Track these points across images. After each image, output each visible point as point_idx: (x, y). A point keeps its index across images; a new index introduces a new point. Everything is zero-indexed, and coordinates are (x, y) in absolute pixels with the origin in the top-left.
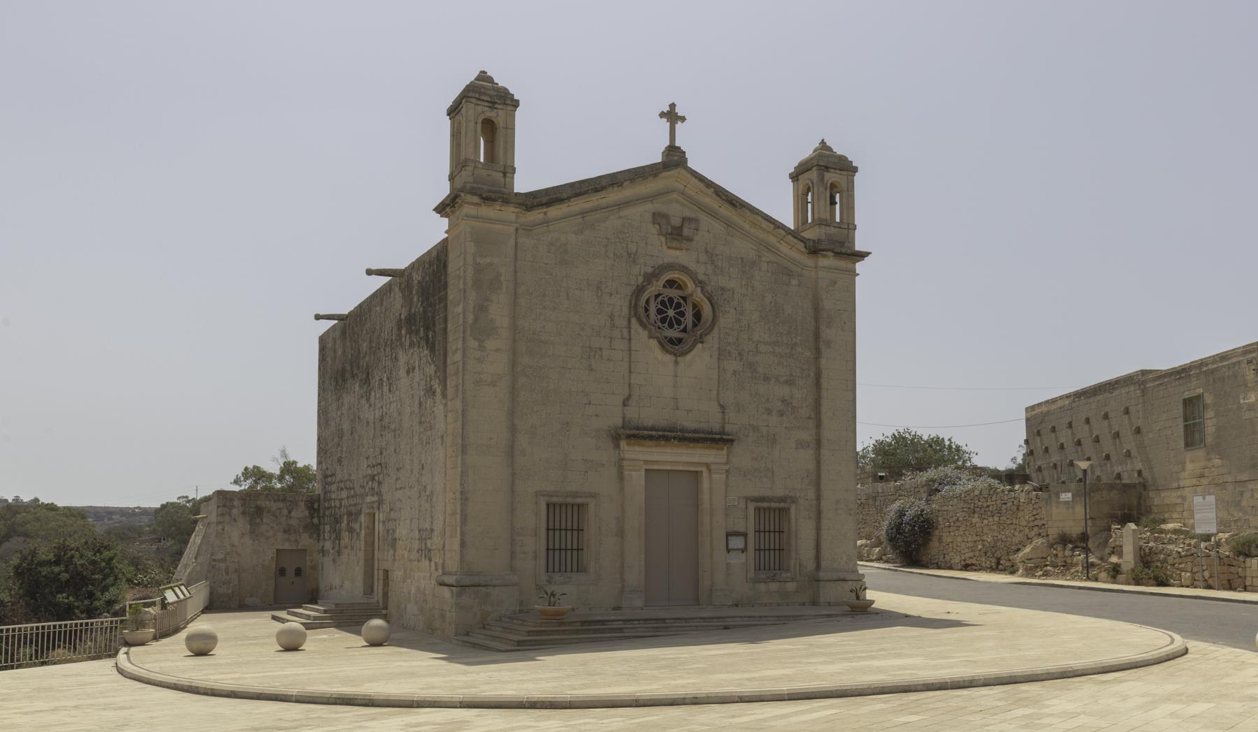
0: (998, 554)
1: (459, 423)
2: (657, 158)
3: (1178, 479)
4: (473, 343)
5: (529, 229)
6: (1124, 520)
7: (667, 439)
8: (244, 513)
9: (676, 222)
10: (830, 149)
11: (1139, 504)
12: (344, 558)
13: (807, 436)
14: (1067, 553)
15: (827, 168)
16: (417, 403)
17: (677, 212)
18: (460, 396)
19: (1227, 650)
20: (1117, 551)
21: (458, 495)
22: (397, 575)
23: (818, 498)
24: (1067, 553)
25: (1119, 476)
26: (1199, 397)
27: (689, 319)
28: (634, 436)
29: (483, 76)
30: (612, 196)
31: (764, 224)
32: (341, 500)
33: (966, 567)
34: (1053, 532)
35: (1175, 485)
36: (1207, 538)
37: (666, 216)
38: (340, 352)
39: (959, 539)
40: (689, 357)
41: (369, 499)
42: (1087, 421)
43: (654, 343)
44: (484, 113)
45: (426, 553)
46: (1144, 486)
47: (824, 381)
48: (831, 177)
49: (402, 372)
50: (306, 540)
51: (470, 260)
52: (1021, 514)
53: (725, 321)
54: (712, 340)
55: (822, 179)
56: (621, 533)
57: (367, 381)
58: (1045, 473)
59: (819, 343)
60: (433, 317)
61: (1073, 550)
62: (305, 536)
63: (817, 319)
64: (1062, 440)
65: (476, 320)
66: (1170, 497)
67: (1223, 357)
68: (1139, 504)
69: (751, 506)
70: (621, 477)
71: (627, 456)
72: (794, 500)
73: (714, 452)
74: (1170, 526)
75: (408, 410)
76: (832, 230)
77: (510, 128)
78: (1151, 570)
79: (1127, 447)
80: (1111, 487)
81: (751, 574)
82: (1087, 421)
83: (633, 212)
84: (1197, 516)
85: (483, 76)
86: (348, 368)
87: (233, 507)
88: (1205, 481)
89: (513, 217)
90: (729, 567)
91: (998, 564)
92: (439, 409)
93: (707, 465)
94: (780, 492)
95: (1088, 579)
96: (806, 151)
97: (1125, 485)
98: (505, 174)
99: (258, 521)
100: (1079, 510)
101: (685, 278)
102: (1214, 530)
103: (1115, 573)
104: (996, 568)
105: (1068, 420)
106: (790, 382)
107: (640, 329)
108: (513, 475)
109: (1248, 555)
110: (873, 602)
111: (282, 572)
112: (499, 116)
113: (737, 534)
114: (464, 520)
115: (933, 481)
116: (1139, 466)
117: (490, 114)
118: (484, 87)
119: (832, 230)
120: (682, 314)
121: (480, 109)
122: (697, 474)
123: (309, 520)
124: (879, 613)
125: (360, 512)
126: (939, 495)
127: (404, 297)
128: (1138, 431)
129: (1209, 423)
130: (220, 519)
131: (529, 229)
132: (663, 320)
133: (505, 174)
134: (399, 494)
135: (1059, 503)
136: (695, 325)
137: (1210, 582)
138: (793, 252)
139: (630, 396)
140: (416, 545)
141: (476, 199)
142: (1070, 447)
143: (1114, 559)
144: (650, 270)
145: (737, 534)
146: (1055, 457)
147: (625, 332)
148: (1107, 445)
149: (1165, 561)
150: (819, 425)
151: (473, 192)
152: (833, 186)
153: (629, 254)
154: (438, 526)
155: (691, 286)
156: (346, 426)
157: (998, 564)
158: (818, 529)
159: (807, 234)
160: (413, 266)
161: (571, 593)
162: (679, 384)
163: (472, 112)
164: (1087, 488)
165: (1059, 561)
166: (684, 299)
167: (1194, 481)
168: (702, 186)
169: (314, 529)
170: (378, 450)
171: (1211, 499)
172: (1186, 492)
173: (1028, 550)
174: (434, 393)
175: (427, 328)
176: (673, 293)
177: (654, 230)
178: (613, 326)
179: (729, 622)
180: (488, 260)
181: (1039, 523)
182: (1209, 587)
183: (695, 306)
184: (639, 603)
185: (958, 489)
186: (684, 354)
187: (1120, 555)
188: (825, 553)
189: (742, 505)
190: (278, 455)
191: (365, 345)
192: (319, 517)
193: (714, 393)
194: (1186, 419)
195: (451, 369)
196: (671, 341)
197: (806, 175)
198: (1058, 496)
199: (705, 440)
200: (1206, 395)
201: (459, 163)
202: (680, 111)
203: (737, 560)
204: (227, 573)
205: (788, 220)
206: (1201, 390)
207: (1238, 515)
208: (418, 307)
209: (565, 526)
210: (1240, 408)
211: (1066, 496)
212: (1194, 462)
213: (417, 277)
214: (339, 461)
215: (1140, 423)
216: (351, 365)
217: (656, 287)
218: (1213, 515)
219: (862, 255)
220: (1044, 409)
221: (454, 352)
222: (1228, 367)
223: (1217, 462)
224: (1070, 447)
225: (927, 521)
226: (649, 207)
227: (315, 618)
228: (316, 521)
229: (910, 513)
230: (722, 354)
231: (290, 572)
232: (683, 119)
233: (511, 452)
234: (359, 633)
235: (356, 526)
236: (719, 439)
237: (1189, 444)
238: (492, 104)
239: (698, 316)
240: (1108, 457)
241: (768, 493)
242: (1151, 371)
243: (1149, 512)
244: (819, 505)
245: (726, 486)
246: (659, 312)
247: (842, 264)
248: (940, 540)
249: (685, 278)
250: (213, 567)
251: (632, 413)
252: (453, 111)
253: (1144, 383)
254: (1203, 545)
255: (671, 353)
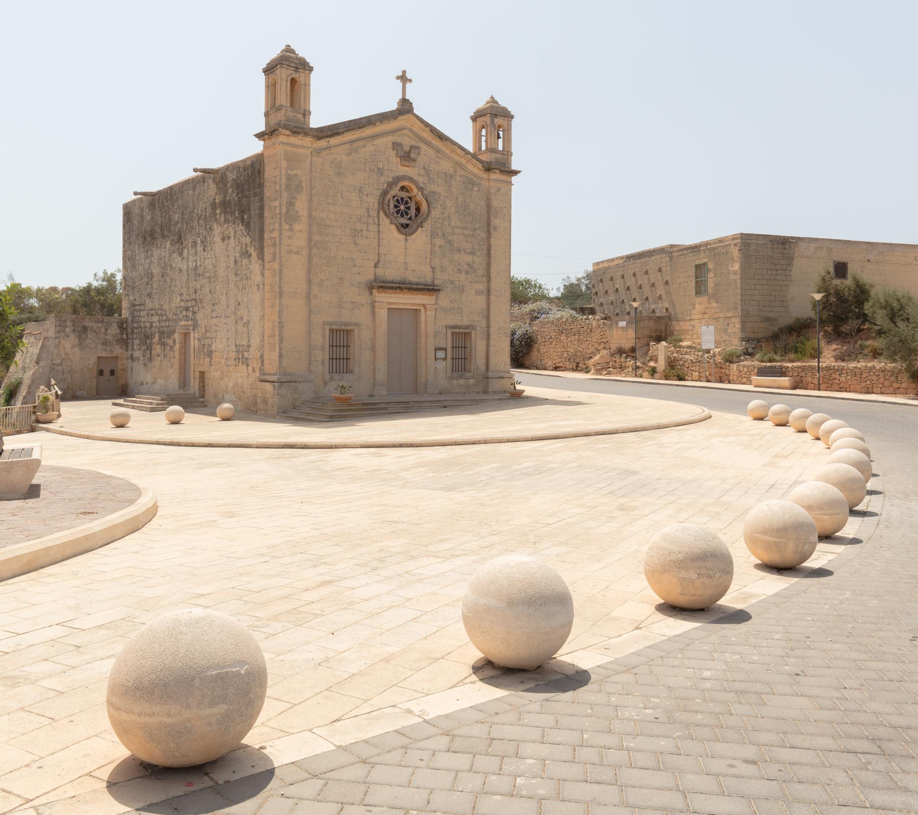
0: (577, 360)
1: (277, 278)
2: (393, 106)
3: (691, 315)
4: (286, 227)
5: (319, 151)
6: (658, 339)
7: (401, 289)
8: (74, 330)
9: (407, 148)
10: (496, 102)
11: (666, 329)
12: (156, 363)
13: (481, 287)
14: (623, 360)
15: (496, 115)
16: (232, 260)
17: (407, 142)
18: (278, 260)
19: (731, 415)
20: (655, 358)
21: (276, 324)
22: (214, 374)
23: (488, 326)
24: (623, 360)
25: (654, 311)
26: (705, 264)
27: (413, 211)
28: (382, 287)
29: (288, 49)
30: (369, 131)
31: (459, 151)
32: (151, 323)
33: (556, 368)
34: (614, 347)
35: (688, 318)
36: (708, 351)
37: (400, 145)
38: (148, 218)
39: (552, 350)
40: (414, 236)
41: (183, 323)
42: (634, 274)
43: (393, 227)
44: (288, 75)
45: (242, 359)
46: (670, 318)
47: (492, 252)
48: (498, 121)
49: (217, 239)
50: (118, 350)
51: (283, 172)
52: (593, 334)
53: (434, 213)
54: (428, 225)
55: (493, 122)
56: (373, 348)
57: (180, 239)
58: (605, 307)
59: (489, 225)
60: (249, 205)
61: (626, 358)
62: (118, 347)
63: (488, 213)
64: (618, 286)
65: (288, 210)
66: (685, 325)
67: (720, 241)
68: (666, 329)
69: (449, 331)
70: (373, 314)
71: (377, 300)
72: (474, 328)
73: (428, 297)
74: (685, 344)
75: (224, 265)
76: (498, 156)
77: (307, 85)
78: (675, 371)
79: (659, 293)
80: (650, 318)
81: (449, 374)
82: (634, 274)
83: (377, 141)
84: (704, 338)
85: (288, 49)
86: (158, 230)
87: (66, 326)
88: (707, 316)
89: (309, 144)
90: (436, 369)
91: (577, 366)
92: (255, 266)
93: (424, 306)
94: (466, 322)
95: (636, 376)
96: (481, 103)
97: (658, 317)
98: (304, 115)
99: (84, 336)
100: (631, 333)
101: (412, 185)
102: (713, 347)
103: (653, 372)
104: (576, 369)
105: (621, 273)
106: (472, 253)
107: (385, 218)
108: (310, 311)
109: (731, 362)
110: (523, 391)
111: (101, 373)
112: (300, 76)
113: (441, 349)
114: (281, 340)
115: (533, 311)
116: (666, 305)
117: (295, 75)
118: (291, 57)
119: (498, 156)
120: (409, 208)
121: (289, 72)
122: (417, 311)
123: (119, 336)
124: (527, 397)
125: (174, 332)
126: (538, 321)
127: (218, 188)
128: (667, 283)
129: (710, 281)
130: (58, 335)
131: (319, 151)
132: (398, 212)
133: (304, 115)
134: (214, 321)
135: (617, 327)
136: (416, 216)
137: (709, 378)
138: (475, 169)
139: (379, 261)
140: (234, 355)
141: (288, 132)
142: (622, 291)
143: (652, 364)
144: (391, 180)
145: (441, 349)
146: (612, 297)
147: (376, 219)
148: (647, 291)
149: (683, 365)
150: (489, 281)
151: (286, 127)
152: (499, 126)
153: (379, 169)
154: (255, 342)
155: (415, 190)
156: (156, 271)
157: (577, 366)
158: (488, 346)
159: (483, 157)
160: (227, 168)
161: (358, 386)
162: (407, 254)
163: (283, 74)
164: (637, 318)
165: (617, 365)
166: (410, 198)
167: (700, 316)
168: (422, 125)
169: (125, 343)
170: (192, 290)
171: (712, 328)
172: (695, 323)
173: (597, 357)
174: (250, 256)
175: (242, 212)
176: (404, 194)
177: (393, 153)
178: (369, 216)
179: (445, 404)
180: (295, 172)
181: (605, 340)
182: (709, 381)
183: (416, 203)
184: (384, 392)
185: (551, 317)
186: (411, 234)
187: (656, 361)
188: (492, 361)
189: (444, 331)
190: (6, 279)
191: (177, 216)
192: (127, 334)
193: (428, 260)
194: (696, 278)
195: (267, 242)
196: (402, 225)
197: (482, 119)
198: (617, 323)
199: (424, 289)
200: (709, 263)
201: (272, 107)
202: (409, 76)
203: (441, 365)
204: (63, 374)
205: (470, 146)
206: (706, 260)
207: (725, 337)
208: (232, 194)
209: (341, 341)
210: (729, 273)
211: (623, 324)
212: (701, 303)
213: (231, 176)
214: (149, 295)
215: (668, 278)
216: (162, 229)
217: (395, 191)
218: (713, 338)
219: (516, 173)
220: (606, 265)
221: (271, 232)
222: (723, 247)
223: (714, 305)
224: (622, 291)
225: (530, 338)
226: (390, 139)
227: (157, 404)
228: (124, 336)
229: (519, 333)
230: (433, 235)
231: (107, 373)
232: (410, 81)
233: (308, 296)
234: (214, 414)
235: (170, 342)
236: (431, 289)
237: (698, 293)
238: (297, 69)
239: (418, 210)
240: (647, 299)
241: (459, 323)
242: (675, 246)
243: (672, 334)
244: (488, 331)
245: (435, 319)
246: (396, 206)
247: (504, 177)
248: (538, 351)
249: (412, 185)
250: (53, 369)
251: (380, 272)
252: (269, 70)
253: (672, 253)
254: (706, 355)
255: (401, 233)
